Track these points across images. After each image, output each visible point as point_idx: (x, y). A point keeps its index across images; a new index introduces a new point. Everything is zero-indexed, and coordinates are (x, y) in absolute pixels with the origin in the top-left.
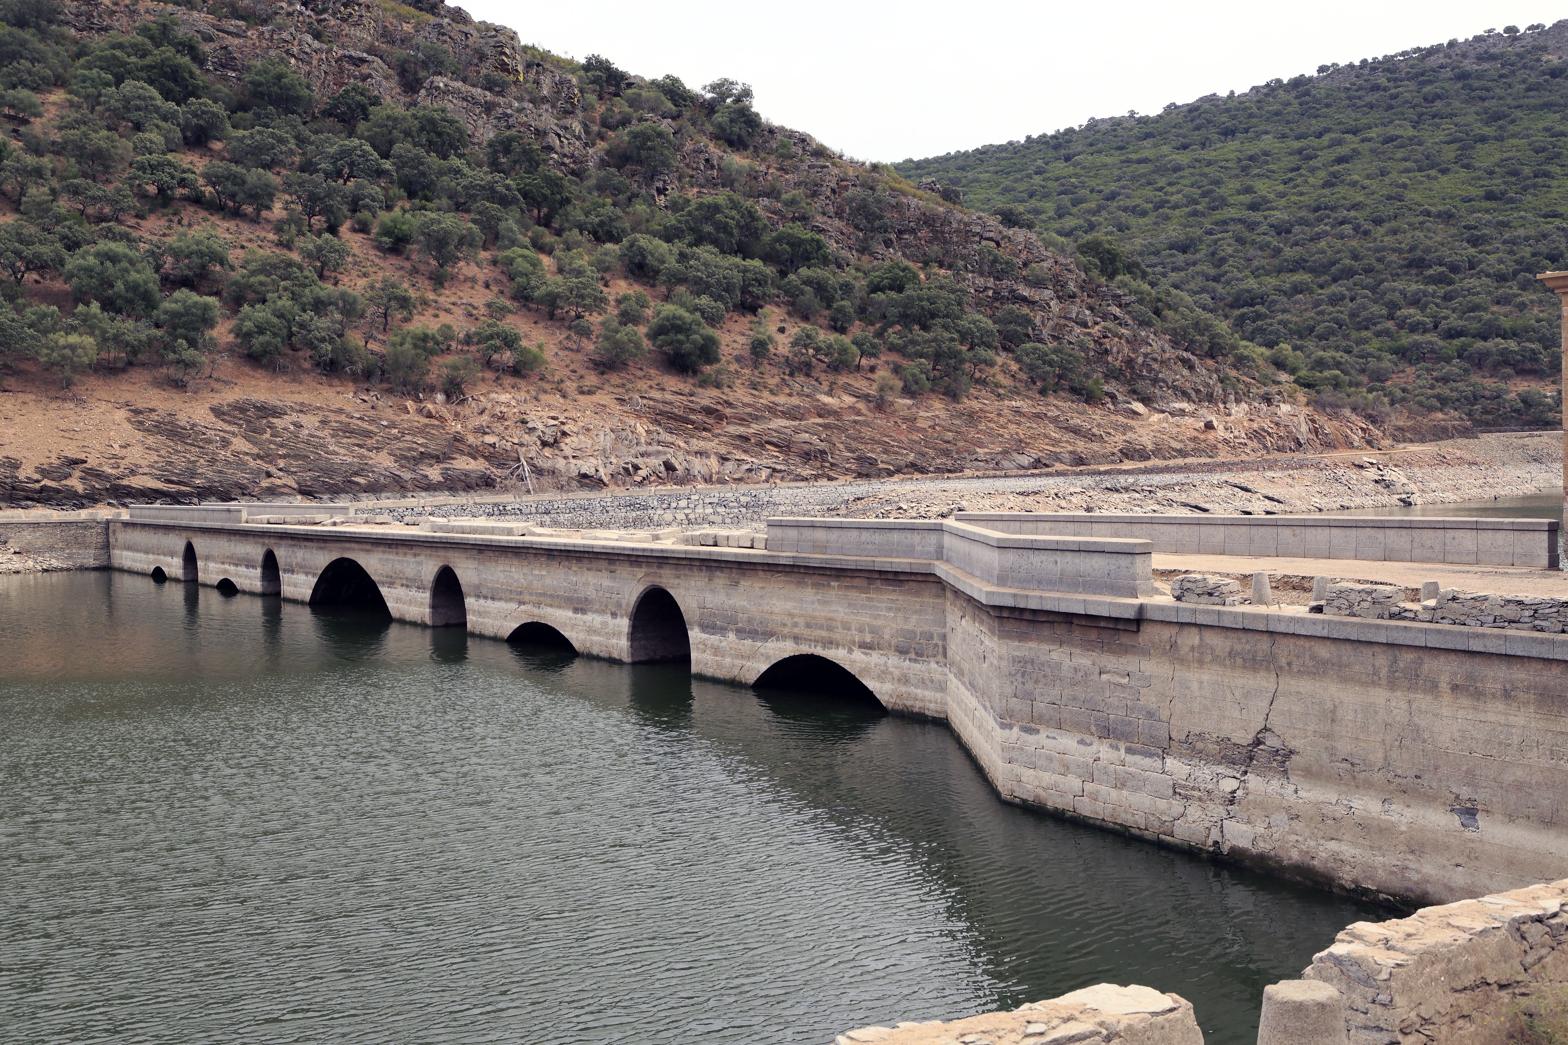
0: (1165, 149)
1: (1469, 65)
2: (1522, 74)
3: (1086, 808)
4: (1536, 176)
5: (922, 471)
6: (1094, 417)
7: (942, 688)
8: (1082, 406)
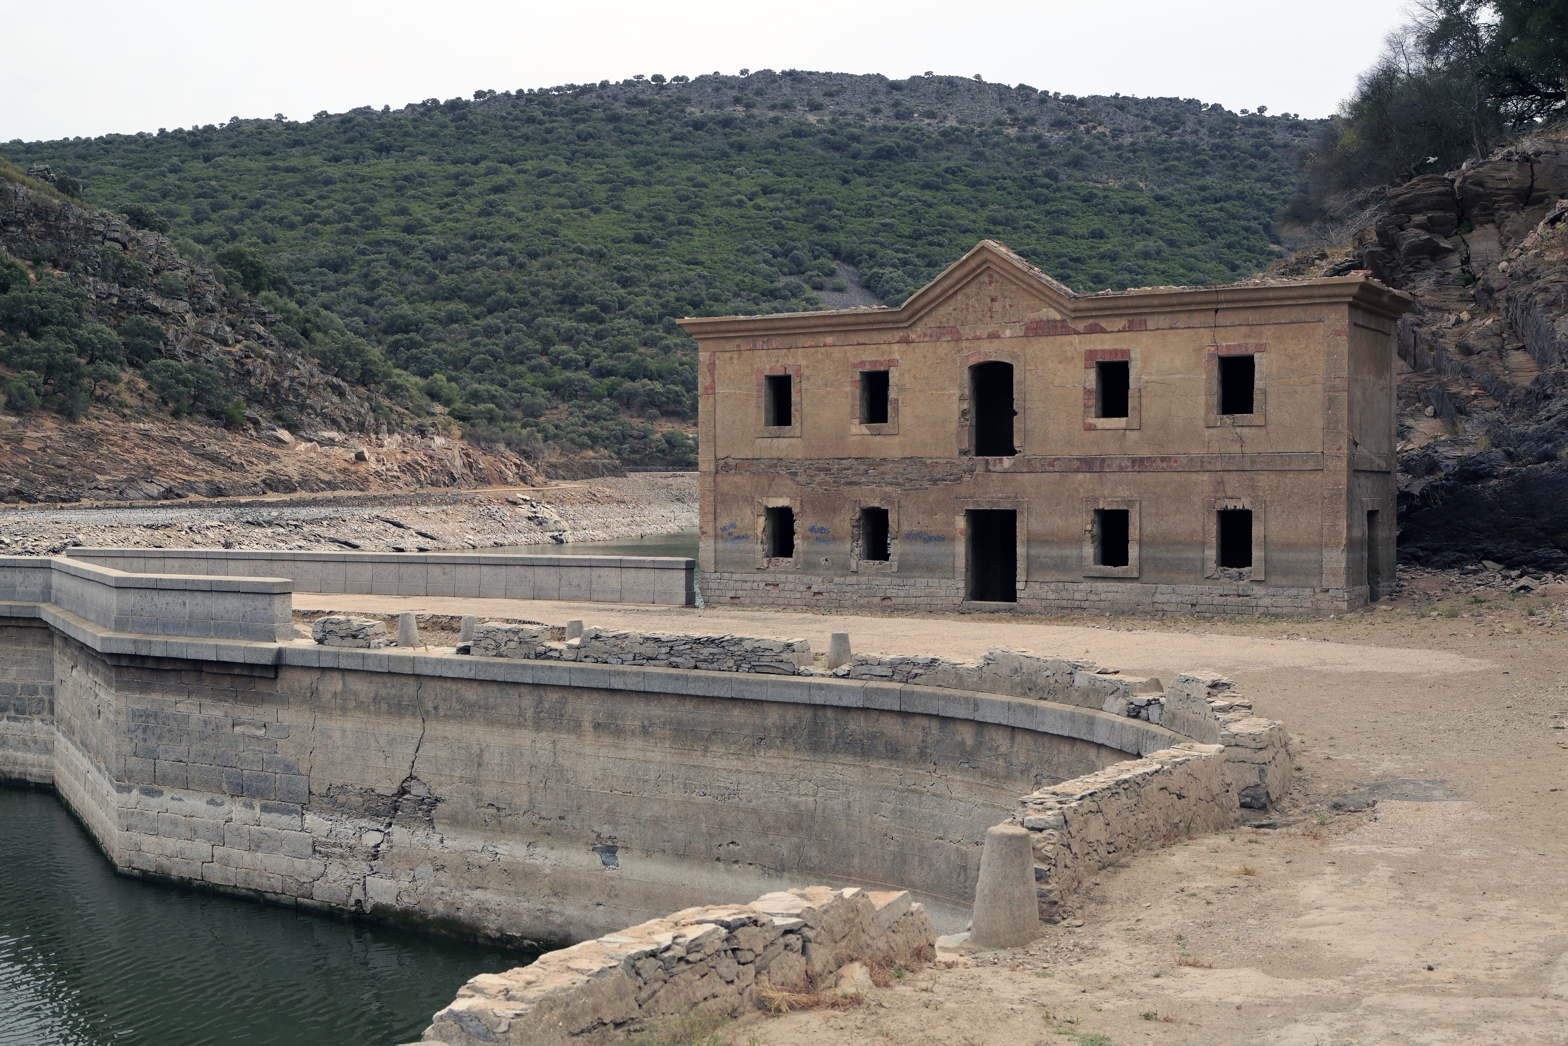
0: (316, 160)
1: (619, 108)
2: (667, 123)
3: (216, 875)
4: (680, 224)
5: (30, 499)
6: (234, 445)
7: (48, 749)
8: (221, 432)
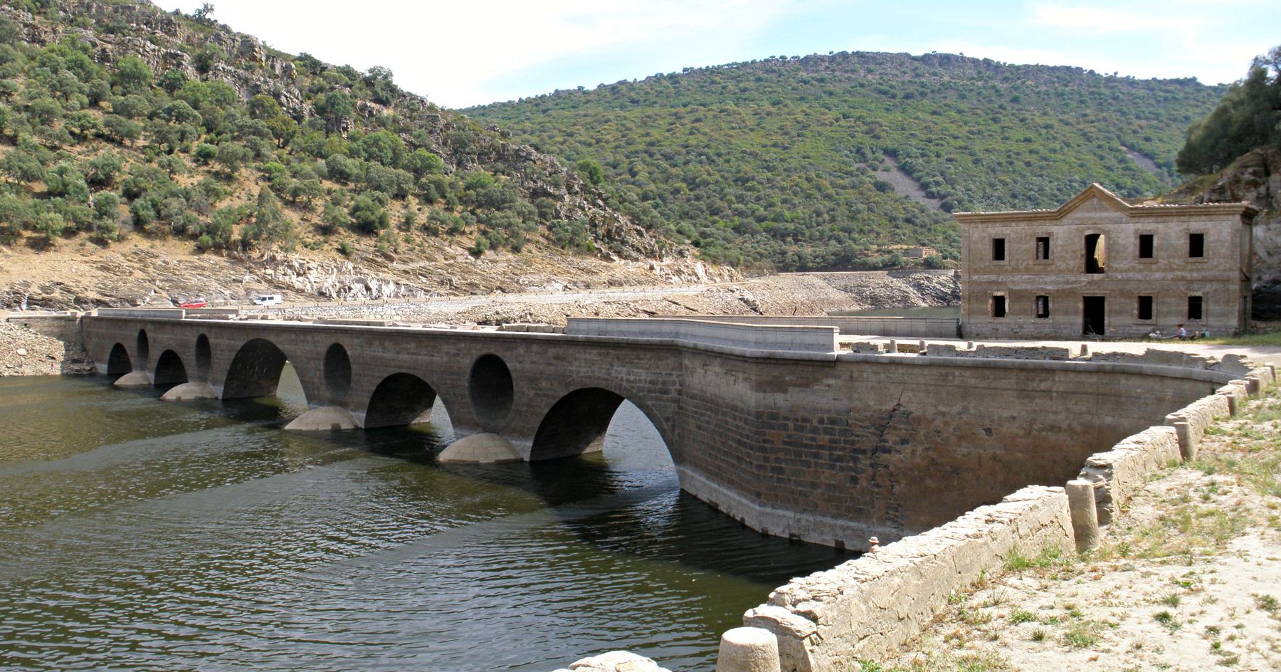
1: (760, 74)
